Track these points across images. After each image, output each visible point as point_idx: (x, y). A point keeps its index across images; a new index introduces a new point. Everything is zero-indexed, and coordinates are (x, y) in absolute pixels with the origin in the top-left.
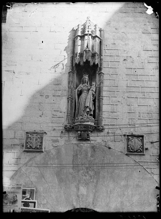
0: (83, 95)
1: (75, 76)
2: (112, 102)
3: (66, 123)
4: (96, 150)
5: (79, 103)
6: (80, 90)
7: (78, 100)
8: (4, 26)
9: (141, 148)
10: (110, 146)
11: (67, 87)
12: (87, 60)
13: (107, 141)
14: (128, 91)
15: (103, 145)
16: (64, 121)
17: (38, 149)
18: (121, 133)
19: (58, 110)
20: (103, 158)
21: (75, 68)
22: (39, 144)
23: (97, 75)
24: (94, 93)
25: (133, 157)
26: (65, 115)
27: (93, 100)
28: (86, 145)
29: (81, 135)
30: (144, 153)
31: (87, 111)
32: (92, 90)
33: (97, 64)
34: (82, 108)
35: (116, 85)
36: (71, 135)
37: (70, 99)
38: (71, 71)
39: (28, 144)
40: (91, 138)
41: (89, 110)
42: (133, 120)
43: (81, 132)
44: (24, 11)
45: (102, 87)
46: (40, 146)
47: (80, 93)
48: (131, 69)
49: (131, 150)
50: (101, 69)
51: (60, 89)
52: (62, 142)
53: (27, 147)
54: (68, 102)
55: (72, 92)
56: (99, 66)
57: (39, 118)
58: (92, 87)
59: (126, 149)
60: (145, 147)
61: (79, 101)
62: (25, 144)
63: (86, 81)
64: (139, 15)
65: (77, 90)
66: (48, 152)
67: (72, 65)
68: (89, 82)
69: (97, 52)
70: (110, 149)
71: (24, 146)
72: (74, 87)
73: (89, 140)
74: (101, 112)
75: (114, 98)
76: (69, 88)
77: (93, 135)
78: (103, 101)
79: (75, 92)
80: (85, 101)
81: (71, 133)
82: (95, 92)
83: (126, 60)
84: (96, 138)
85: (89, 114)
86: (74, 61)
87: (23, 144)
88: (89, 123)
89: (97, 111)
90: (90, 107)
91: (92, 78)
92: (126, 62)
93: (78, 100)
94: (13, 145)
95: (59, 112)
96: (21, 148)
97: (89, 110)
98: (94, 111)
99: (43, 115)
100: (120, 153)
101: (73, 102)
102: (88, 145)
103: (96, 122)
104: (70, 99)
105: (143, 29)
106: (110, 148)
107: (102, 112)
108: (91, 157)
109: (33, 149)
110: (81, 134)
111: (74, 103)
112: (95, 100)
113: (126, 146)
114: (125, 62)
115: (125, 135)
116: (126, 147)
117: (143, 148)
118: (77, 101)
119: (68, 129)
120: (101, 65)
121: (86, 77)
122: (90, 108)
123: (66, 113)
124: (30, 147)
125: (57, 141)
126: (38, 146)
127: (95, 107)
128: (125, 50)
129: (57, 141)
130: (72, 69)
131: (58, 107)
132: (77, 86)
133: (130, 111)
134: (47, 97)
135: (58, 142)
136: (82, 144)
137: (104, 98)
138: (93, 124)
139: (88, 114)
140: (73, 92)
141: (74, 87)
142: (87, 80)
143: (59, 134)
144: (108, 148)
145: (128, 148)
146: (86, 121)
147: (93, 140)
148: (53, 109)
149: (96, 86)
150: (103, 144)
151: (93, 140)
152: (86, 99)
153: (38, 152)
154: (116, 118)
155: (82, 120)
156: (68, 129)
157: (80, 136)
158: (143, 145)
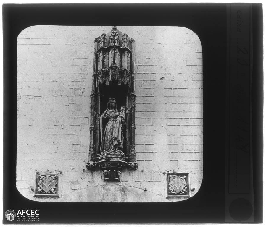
0: (110, 124)
5: (104, 134)
19: (77, 143)
32: (121, 117)
34: (108, 139)
39: (39, 188)
49: (173, 192)
67: (95, 86)
70: (146, 191)
72: (97, 113)
81: (96, 172)
95: (79, 146)
102: (118, 187)
109: (46, 193)
117: (187, 189)
118: (101, 131)
122: (119, 140)
132: (102, 112)
156: (91, 169)
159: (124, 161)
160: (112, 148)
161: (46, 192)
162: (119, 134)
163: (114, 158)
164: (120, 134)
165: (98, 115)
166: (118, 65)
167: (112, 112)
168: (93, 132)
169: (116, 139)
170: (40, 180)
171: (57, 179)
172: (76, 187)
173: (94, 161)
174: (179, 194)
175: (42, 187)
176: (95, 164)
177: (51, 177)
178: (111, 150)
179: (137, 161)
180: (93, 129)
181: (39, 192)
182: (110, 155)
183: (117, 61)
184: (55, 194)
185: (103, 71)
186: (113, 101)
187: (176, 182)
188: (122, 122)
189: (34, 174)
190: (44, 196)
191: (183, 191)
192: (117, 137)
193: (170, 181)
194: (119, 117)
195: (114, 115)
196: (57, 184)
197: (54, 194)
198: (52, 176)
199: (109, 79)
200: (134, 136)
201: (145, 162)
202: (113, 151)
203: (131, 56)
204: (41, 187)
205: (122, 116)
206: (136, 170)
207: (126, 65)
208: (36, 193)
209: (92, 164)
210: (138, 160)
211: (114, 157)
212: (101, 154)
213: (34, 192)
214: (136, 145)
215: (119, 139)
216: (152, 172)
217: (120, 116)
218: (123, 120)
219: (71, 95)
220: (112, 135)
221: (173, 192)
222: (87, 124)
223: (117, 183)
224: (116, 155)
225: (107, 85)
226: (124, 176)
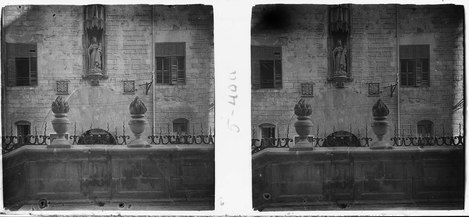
0: (94, 53)
1: (87, 38)
2: (113, 57)
3: (83, 74)
4: (104, 91)
5: (91, 59)
6: (91, 49)
7: (90, 57)
8: (456, 5)
9: (378, 92)
11: (82, 47)
12: (340, 29)
13: (110, 85)
16: (81, 73)
17: (65, 92)
18: (120, 80)
20: (108, 97)
23: (103, 36)
24: (101, 51)
25: (127, 95)
26: (81, 68)
27: (100, 56)
28: (97, 88)
29: (338, 85)
30: (134, 92)
33: (103, 28)
34: (93, 63)
35: (361, 47)
37: (84, 56)
38: (329, 37)
39: (303, 92)
40: (100, 84)
41: (343, 67)
42: (373, 72)
43: (338, 82)
45: (351, 49)
47: (91, 51)
48: (126, 31)
50: (105, 32)
52: (325, 90)
53: (303, 94)
54: (83, 58)
55: (85, 51)
56: (104, 30)
58: (99, 46)
59: (368, 93)
60: (136, 88)
62: (301, 92)
63: (95, 42)
65: (89, 49)
66: (317, 97)
67: (85, 30)
68: (97, 43)
69: (346, 21)
71: (301, 93)
72: (331, 49)
73: (98, 85)
74: (106, 65)
76: (83, 47)
77: (101, 81)
78: (108, 57)
79: (333, 53)
82: (347, 53)
84: (104, 84)
88: (98, 74)
89: (103, 64)
91: (99, 39)
92: (123, 25)
93: (90, 57)
94: (294, 93)
95: (77, 66)
96: (54, 92)
97: (343, 67)
98: (346, 67)
100: (364, 95)
101: (86, 58)
102: (343, 91)
103: (103, 72)
104: (84, 56)
106: (112, 90)
110: (93, 81)
111: (87, 59)
113: (368, 90)
114: (122, 25)
115: (122, 81)
116: (368, 91)
117: (134, 89)
118: (334, 60)
119: (84, 78)
120: (105, 29)
121: (95, 39)
123: (82, 66)
124: (305, 93)
125: (323, 89)
126: (65, 90)
130: (85, 33)
132: (334, 49)
133: (126, 63)
136: (339, 91)
137: (353, 57)
138: (100, 74)
139: (97, 67)
140: (86, 50)
142: (95, 41)
143: (79, 82)
144: (356, 93)
145: (124, 89)
147: (101, 85)
148: (73, 64)
149: (102, 45)
150: (353, 90)
151: (101, 85)
152: (95, 56)
156: (84, 78)
157: (338, 85)
158: (134, 87)
161: (62, 91)
168: (329, 60)
174: (130, 92)
185: (89, 20)
186: (95, 39)
187: (128, 85)
188: (345, 55)
199: (92, 26)
203: (349, 12)
217: (344, 51)
223: (343, 89)
226: (101, 83)
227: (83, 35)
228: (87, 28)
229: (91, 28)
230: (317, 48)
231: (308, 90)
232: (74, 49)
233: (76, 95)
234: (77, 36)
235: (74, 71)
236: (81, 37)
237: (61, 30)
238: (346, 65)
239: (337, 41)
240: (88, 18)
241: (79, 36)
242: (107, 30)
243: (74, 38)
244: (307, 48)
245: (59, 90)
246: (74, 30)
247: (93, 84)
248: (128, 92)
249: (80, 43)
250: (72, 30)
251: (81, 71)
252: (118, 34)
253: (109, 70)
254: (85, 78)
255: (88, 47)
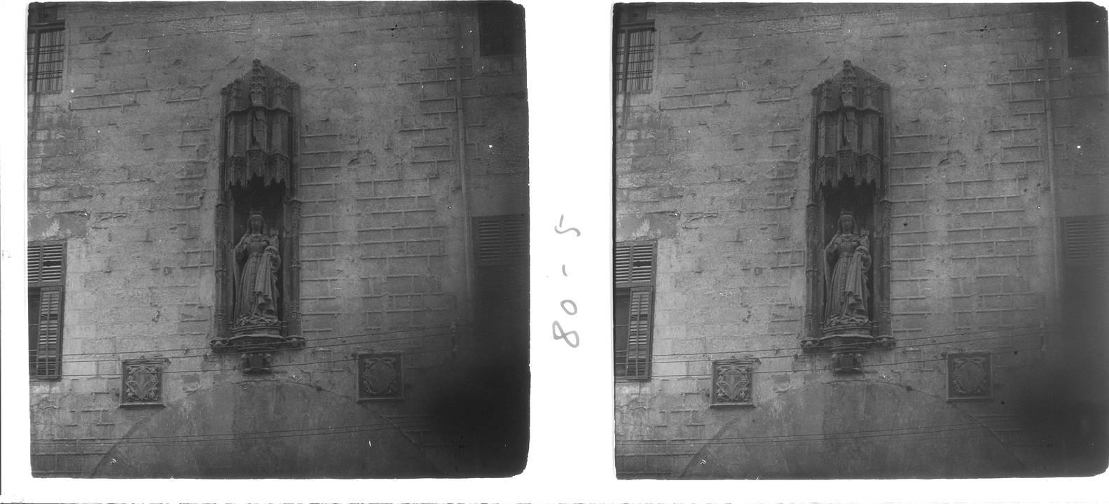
3: (214, 334)
10: (909, 385)
12: (845, 176)
14: (362, 243)
15: (304, 382)
19: (194, 303)
21: (230, 194)
22: (154, 388)
28: (262, 384)
31: (260, 302)
32: (861, 250)
34: (247, 296)
36: (227, 363)
39: (718, 391)
43: (248, 354)
44: (695, 52)
46: (747, 392)
49: (960, 391)
51: (197, 250)
57: (151, 325)
61: (833, 277)
62: (711, 391)
64: (977, 37)
67: (814, 188)
70: (321, 392)
72: (229, 242)
75: (328, 262)
80: (255, 280)
81: (227, 357)
83: (357, 161)
85: (855, 311)
86: (818, 179)
87: (118, 390)
90: (266, 294)
92: (946, 167)
95: (197, 307)
97: (263, 302)
99: (752, 317)
101: (228, 281)
105: (987, 75)
107: (889, 299)
108: (865, 413)
109: (730, 401)
112: (873, 272)
122: (858, 296)
123: (805, 308)
127: (873, 289)
128: (944, 134)
129: (195, 379)
131: (786, 294)
132: (827, 241)
134: (167, 273)
135: (199, 380)
141: (229, 242)
144: (905, 390)
146: (257, 329)
148: (182, 301)
153: (743, 407)
154: (333, 314)
155: (248, 326)
157: (838, 364)
159: (277, 334)
160: (255, 312)
162: (267, 283)
163: (257, 331)
164: (859, 282)
165: (820, 245)
166: (264, 147)
167: (255, 239)
169: (851, 293)
170: (719, 375)
171: (159, 372)
172: (194, 387)
173: (813, 337)
175: (725, 389)
176: (816, 342)
177: (150, 369)
178: (844, 315)
179: (895, 332)
180: (811, 273)
181: (720, 399)
182: (840, 326)
183: (262, 138)
184: (748, 401)
189: (119, 365)
190: (138, 406)
191: (389, 388)
192: (853, 291)
193: (955, 368)
194: (858, 250)
195: (849, 245)
196: (751, 382)
197: (155, 401)
198: (150, 367)
199: (246, 176)
200: (298, 284)
201: (317, 333)
202: (846, 316)
204: (132, 389)
205: (864, 248)
206: (891, 349)
207: (870, 143)
208: (713, 402)
209: (810, 343)
210: (896, 330)
211: (257, 329)
212: (826, 323)
213: (710, 399)
214: (300, 301)
215: (857, 294)
216: (922, 354)
218: (274, 256)
219: (772, 207)
220: (845, 286)
221: (960, 391)
222: (211, 264)
223: (857, 377)
224: (260, 325)
225: (859, 186)
227: (808, 207)
228: (821, 183)
229: (243, 184)
230: (183, 239)
231: (735, 383)
232: (186, 251)
233: (190, 408)
234: (789, 208)
235: (186, 325)
236: (803, 213)
237: (738, 193)
238: (867, 295)
239: (839, 217)
240: (235, 153)
241: (206, 209)
242: (891, 186)
243: (187, 216)
244: (148, 244)
245: (130, 394)
246: (778, 192)
247: (248, 369)
248: (376, 396)
249: (799, 232)
250: (776, 192)
251: (798, 324)
252: (931, 197)
253: (898, 317)
254: (812, 349)
255: (235, 244)
